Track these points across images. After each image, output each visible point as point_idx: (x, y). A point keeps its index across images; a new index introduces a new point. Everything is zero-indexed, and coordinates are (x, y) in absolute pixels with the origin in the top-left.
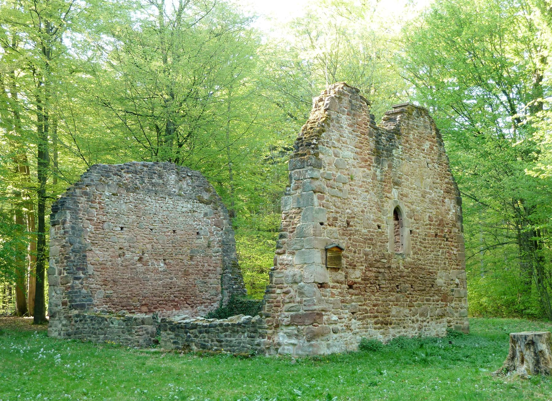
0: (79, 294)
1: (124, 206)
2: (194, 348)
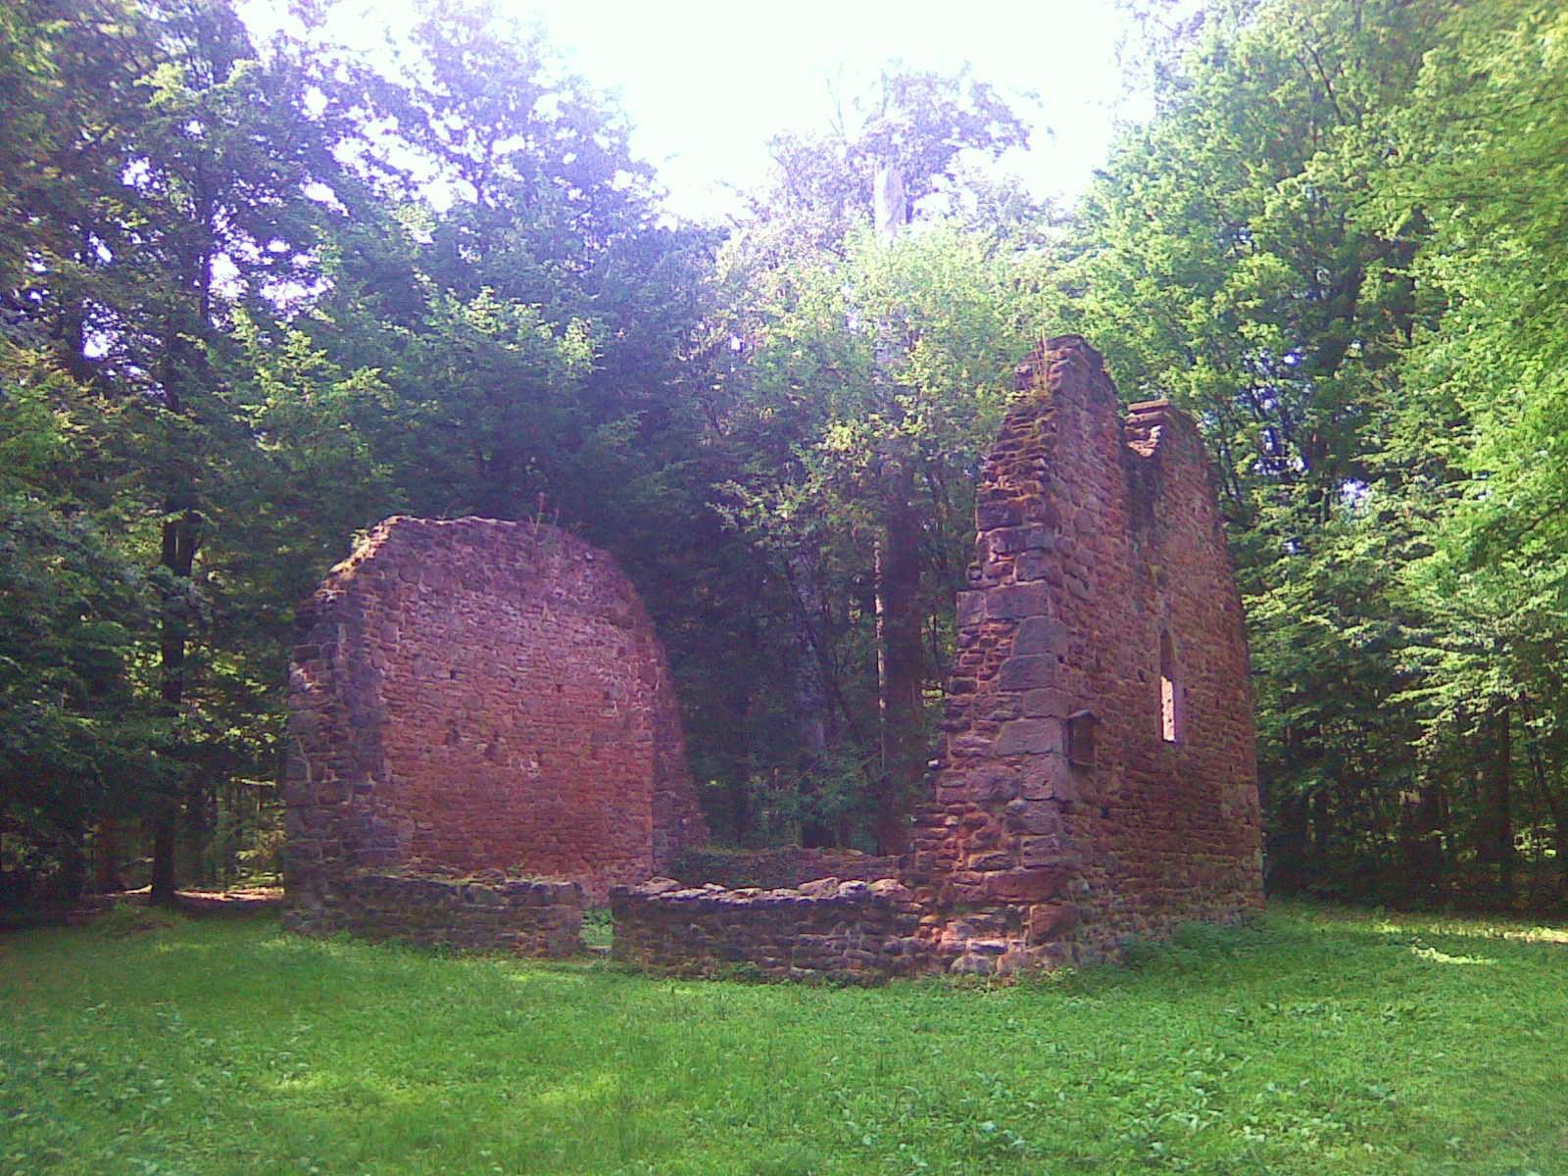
0: (367, 826)
1: (457, 621)
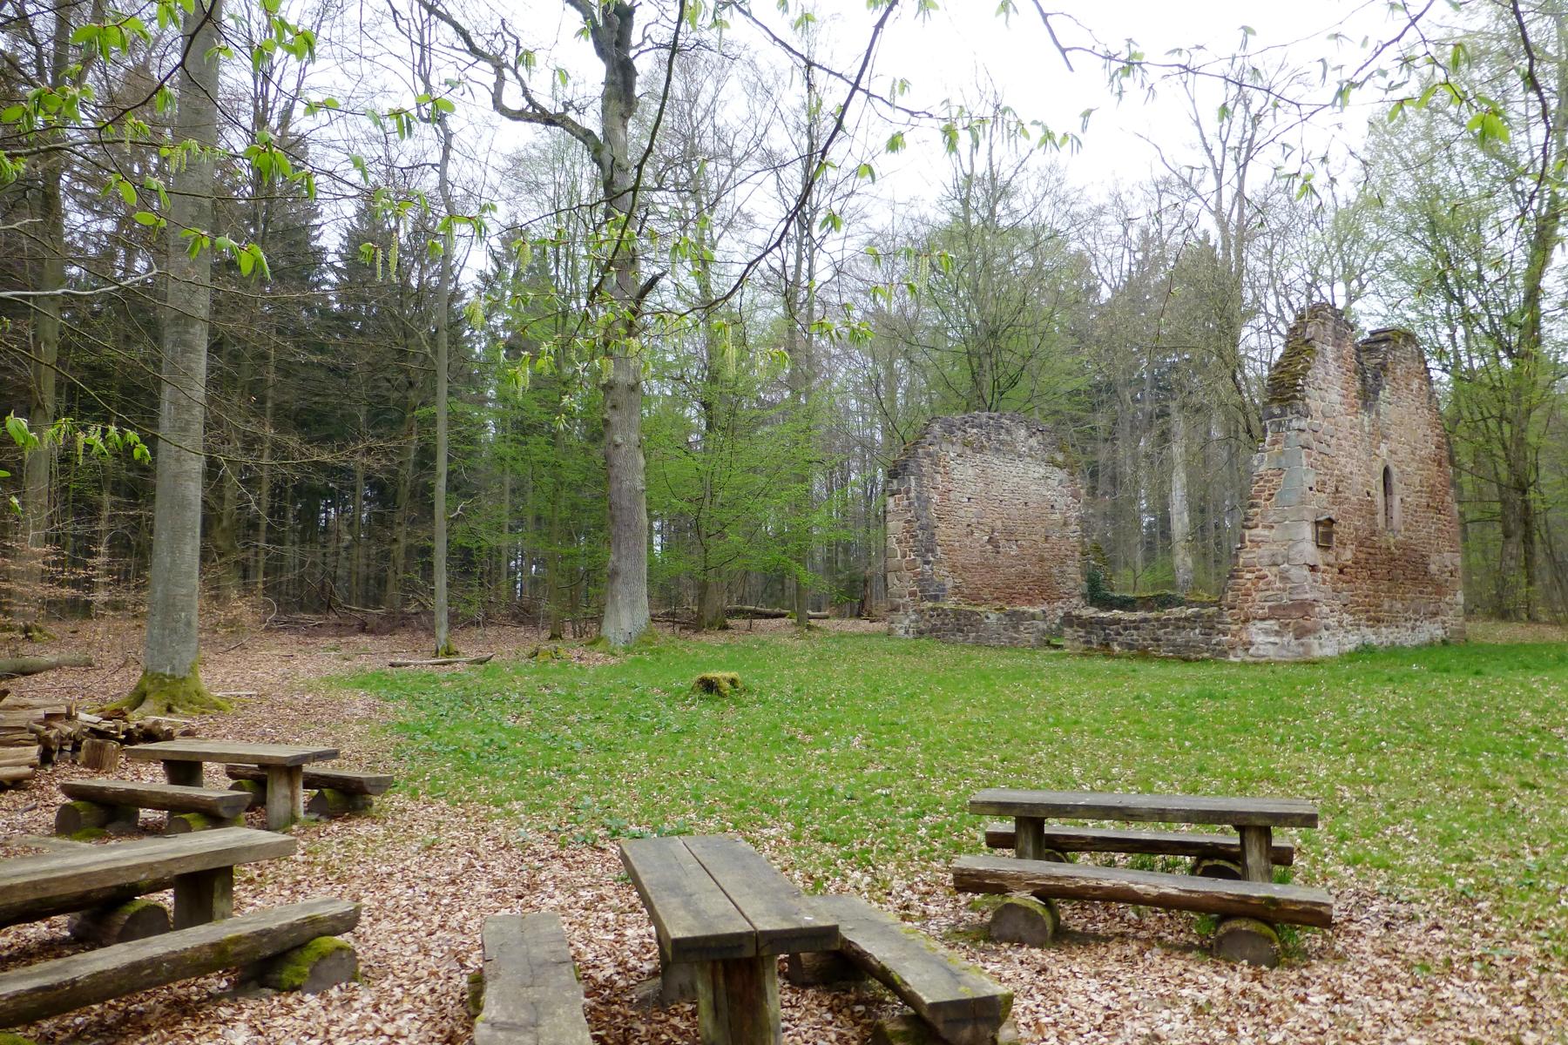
2: (1117, 648)
